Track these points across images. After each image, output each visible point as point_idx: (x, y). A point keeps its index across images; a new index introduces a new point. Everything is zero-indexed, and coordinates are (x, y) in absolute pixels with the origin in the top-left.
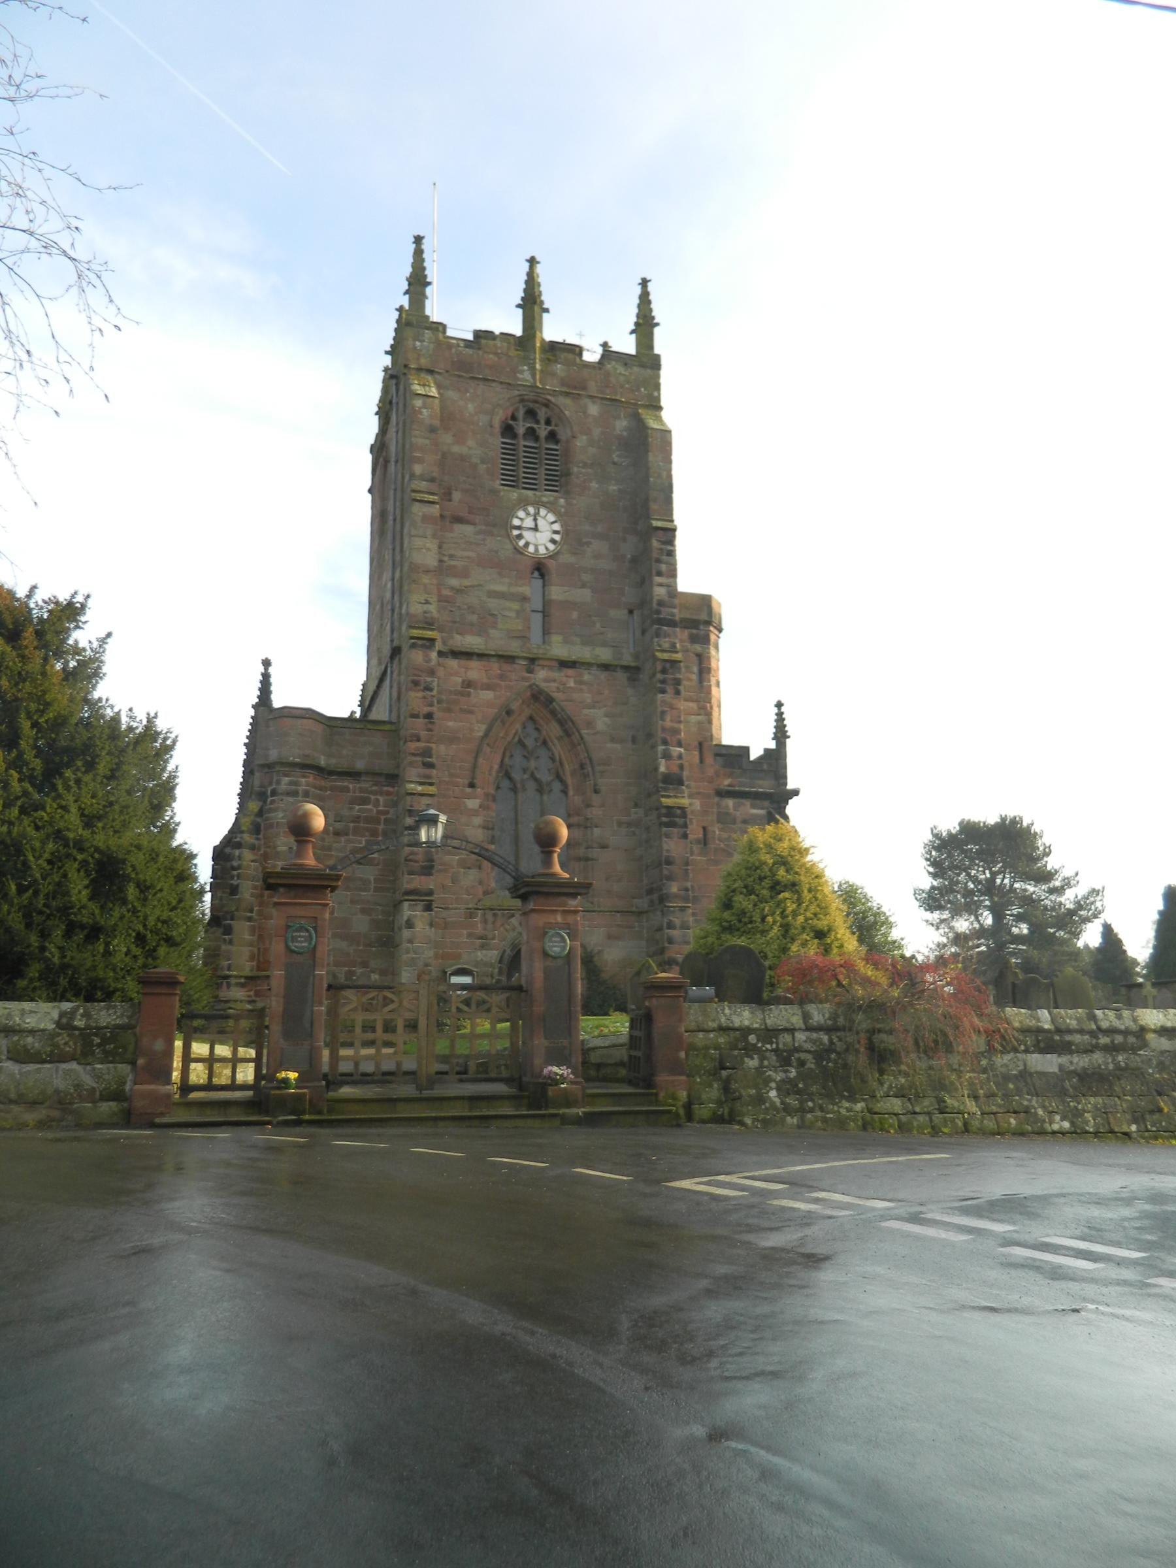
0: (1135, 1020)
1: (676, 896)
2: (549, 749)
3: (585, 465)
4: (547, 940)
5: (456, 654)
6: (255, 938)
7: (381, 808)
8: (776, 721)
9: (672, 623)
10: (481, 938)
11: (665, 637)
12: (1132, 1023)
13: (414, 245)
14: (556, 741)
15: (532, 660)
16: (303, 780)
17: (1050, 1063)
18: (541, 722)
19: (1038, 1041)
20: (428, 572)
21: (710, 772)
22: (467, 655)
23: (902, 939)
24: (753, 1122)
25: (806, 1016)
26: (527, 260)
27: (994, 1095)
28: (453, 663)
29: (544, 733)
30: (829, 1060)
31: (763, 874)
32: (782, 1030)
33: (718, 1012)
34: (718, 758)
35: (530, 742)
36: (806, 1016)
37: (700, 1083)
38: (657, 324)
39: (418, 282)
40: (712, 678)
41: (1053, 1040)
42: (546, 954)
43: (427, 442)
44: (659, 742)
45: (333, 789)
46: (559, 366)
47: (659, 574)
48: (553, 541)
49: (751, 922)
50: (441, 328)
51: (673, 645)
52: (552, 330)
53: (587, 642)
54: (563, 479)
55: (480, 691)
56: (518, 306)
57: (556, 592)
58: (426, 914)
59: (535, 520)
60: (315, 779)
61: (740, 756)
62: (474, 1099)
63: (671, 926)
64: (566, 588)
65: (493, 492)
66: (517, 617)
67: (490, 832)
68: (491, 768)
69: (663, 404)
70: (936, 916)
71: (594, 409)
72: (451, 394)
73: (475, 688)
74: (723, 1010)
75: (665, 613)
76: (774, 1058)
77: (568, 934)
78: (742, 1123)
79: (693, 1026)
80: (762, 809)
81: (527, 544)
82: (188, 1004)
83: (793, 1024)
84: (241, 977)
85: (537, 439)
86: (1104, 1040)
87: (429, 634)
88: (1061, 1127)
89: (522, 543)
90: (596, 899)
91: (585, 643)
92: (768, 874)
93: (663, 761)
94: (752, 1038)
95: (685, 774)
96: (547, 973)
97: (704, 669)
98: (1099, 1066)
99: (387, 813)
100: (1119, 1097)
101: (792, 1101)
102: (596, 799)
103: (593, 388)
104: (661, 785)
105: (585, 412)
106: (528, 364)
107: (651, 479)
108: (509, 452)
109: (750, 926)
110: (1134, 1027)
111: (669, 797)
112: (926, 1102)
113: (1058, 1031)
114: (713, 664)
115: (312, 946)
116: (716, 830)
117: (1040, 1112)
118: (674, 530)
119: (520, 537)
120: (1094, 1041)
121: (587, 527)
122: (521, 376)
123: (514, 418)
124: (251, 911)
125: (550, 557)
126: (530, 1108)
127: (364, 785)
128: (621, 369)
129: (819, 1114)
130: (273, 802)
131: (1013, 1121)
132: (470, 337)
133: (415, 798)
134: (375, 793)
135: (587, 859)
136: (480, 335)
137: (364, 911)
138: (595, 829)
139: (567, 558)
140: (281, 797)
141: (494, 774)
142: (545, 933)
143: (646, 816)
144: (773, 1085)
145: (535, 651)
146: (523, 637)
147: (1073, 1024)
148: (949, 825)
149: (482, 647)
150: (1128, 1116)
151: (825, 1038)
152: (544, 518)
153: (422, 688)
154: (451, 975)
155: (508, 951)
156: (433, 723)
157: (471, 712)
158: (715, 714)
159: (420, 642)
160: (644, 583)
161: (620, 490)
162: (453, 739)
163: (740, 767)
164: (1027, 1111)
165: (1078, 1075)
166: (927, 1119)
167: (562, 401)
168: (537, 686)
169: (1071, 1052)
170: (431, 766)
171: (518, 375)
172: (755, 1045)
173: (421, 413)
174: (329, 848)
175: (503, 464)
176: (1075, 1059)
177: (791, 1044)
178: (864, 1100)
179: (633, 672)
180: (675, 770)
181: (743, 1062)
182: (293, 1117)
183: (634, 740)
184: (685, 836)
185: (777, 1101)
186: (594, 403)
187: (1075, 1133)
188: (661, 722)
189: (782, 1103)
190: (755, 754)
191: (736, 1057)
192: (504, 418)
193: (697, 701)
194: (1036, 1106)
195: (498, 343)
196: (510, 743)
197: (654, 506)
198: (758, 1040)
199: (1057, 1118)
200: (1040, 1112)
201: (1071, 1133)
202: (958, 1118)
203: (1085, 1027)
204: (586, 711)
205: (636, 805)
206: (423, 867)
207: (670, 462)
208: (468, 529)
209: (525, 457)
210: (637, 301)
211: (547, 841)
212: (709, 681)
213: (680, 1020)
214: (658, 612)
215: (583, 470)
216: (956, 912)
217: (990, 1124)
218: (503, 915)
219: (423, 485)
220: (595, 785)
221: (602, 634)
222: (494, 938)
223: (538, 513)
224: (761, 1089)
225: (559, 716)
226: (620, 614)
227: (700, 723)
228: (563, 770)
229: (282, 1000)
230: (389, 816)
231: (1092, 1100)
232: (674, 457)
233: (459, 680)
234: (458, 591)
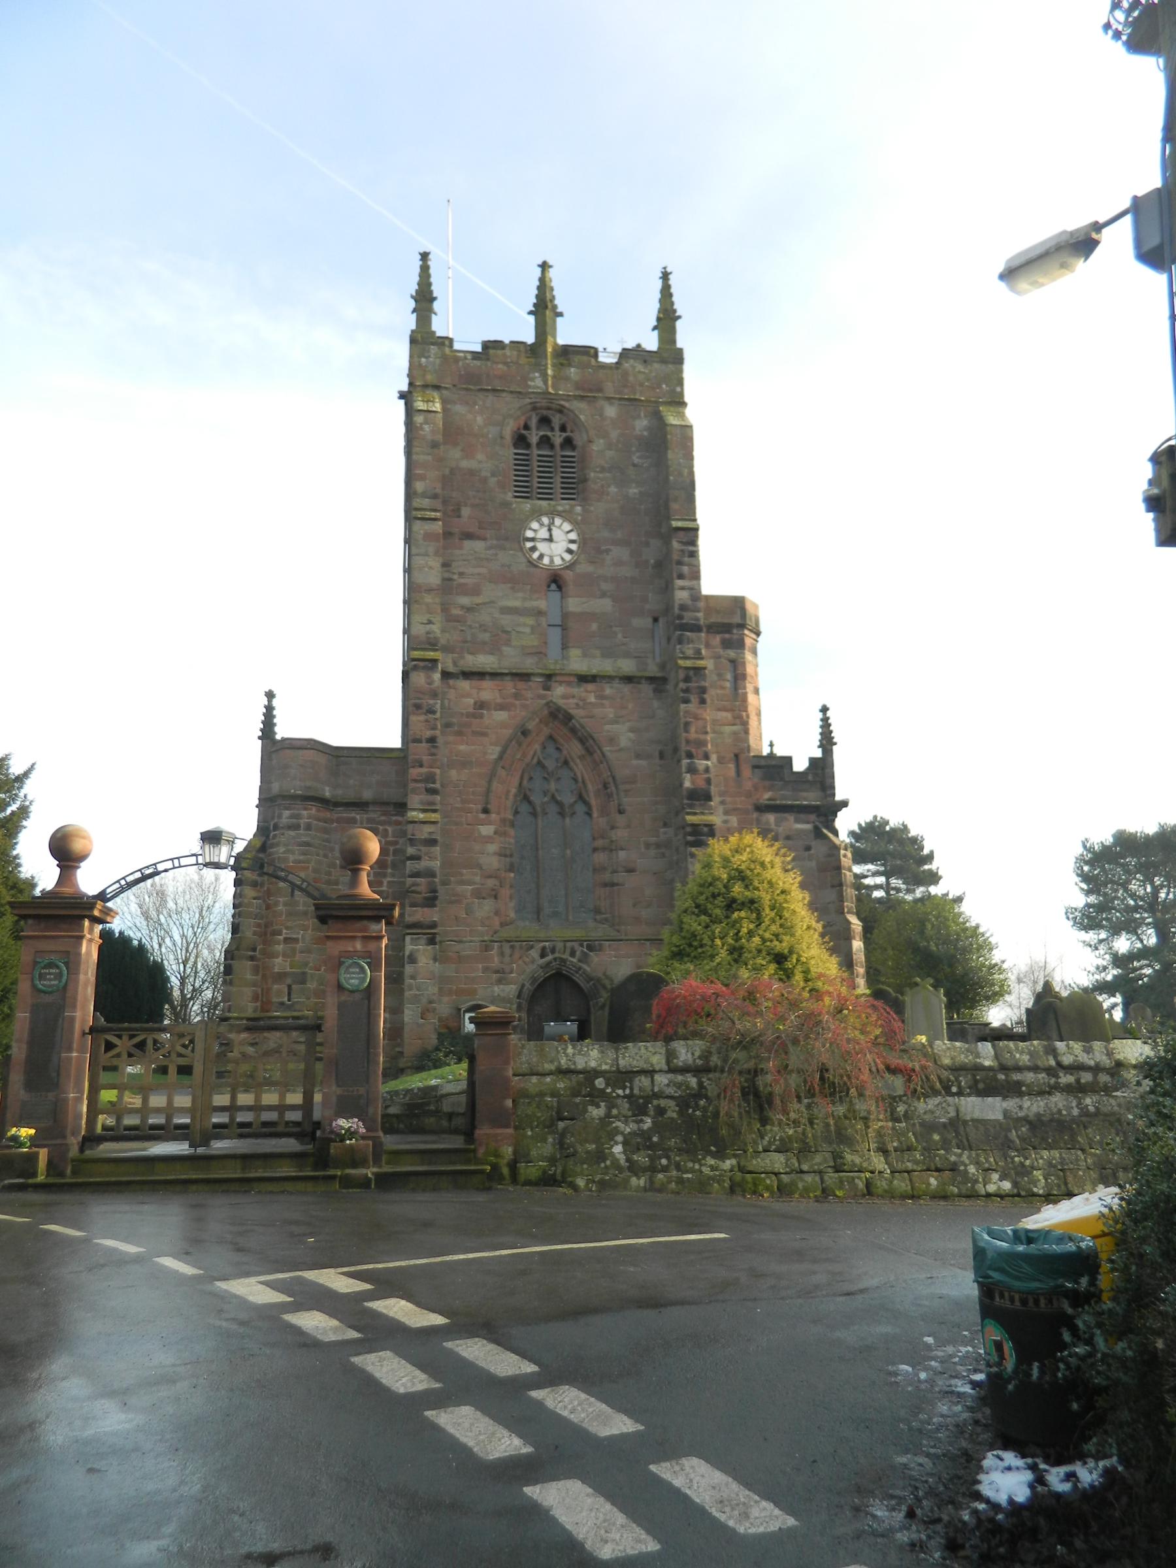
0: (1109, 1054)
2: (571, 769)
3: (603, 470)
4: (342, 970)
5: (467, 675)
6: (259, 977)
7: (390, 839)
8: (821, 727)
9: (696, 628)
10: (497, 972)
11: (688, 643)
12: (1104, 1057)
13: (421, 263)
14: (578, 761)
15: (549, 677)
16: (305, 813)
17: (992, 1109)
18: (561, 740)
19: (976, 1082)
20: (429, 590)
21: (748, 785)
22: (480, 675)
23: (1003, 962)
24: (587, 1184)
25: (670, 1055)
26: (539, 266)
27: (910, 1149)
28: (465, 685)
29: (565, 752)
30: (697, 1107)
31: (716, 891)
32: (637, 1072)
33: (558, 1052)
34: (756, 770)
35: (550, 764)
36: (670, 1055)
37: (532, 1137)
38: (679, 317)
39: (424, 299)
40: (748, 685)
41: (996, 1080)
42: (340, 987)
43: (430, 458)
44: (683, 754)
45: (338, 821)
46: (572, 370)
47: (681, 576)
48: (569, 551)
49: (702, 946)
50: (447, 342)
51: (698, 652)
52: (566, 334)
53: (608, 653)
54: (581, 486)
55: (493, 712)
56: (530, 313)
57: (574, 604)
58: (429, 947)
59: (550, 530)
60: (318, 811)
61: (781, 767)
62: (247, 1159)
64: (584, 600)
65: (506, 504)
66: (532, 633)
67: (508, 859)
68: (508, 792)
69: (686, 399)
70: (1091, 936)
71: (611, 411)
72: (459, 408)
73: (489, 709)
74: (565, 1049)
75: (688, 617)
76: (627, 1106)
77: (369, 964)
78: (575, 1188)
79: (524, 1068)
80: (808, 823)
81: (541, 556)
82: (795, 1041)
83: (652, 1065)
84: (242, 1019)
85: (552, 447)
86: (1066, 1079)
87: (431, 655)
88: (999, 1188)
89: (536, 555)
90: (623, 927)
91: (604, 656)
92: (723, 890)
93: (688, 775)
94: (600, 1083)
95: (713, 790)
96: (341, 1006)
97: (739, 676)
98: (1060, 1111)
99: (396, 843)
100: (1083, 1150)
101: (641, 1158)
102: (621, 820)
103: (609, 389)
104: (686, 801)
105: (601, 415)
106: (540, 371)
107: (671, 478)
108: (522, 463)
109: (700, 950)
110: (1106, 1062)
111: (695, 814)
112: (818, 1158)
113: (1004, 1068)
114: (749, 669)
115: (62, 984)
117: (972, 1169)
118: (696, 530)
119: (534, 549)
120: (1053, 1081)
121: (606, 534)
122: (532, 384)
123: (526, 427)
124: (254, 950)
125: (567, 568)
126: (315, 1169)
127: (372, 815)
128: (640, 367)
129: (674, 1173)
130: (275, 836)
131: (933, 1181)
132: (478, 348)
133: (416, 825)
135: (613, 885)
136: (487, 345)
139: (584, 568)
140: (282, 831)
141: (511, 797)
142: (341, 964)
144: (620, 1138)
145: (552, 667)
146: (540, 654)
147: (1025, 1059)
148: (1103, 836)
149: (495, 666)
150: (1094, 1175)
151: (693, 1081)
152: (559, 527)
153: (424, 711)
154: (465, 1012)
155: (527, 985)
156: (436, 747)
157: (484, 734)
158: (753, 722)
159: (422, 664)
160: (667, 589)
161: (640, 492)
162: (464, 764)
163: (782, 779)
164: (953, 1168)
165: (1030, 1123)
166: (817, 1178)
167: (576, 406)
168: (554, 703)
169: (1021, 1094)
171: (529, 383)
172: (603, 1091)
173: (422, 429)
175: (516, 475)
176: (1026, 1102)
177: (649, 1089)
178: (735, 1156)
179: (658, 683)
180: (701, 784)
181: (586, 1111)
182: (21, 1181)
183: (662, 755)
185: (622, 1158)
186: (611, 404)
187: (1019, 1195)
188: (684, 735)
189: (628, 1160)
191: (577, 1105)
192: (515, 429)
193: (732, 710)
194: (967, 1162)
195: (508, 352)
196: (528, 765)
197: (674, 506)
198: (607, 1085)
199: (995, 1176)
200: (972, 1169)
201: (1013, 1196)
202: (859, 1178)
203: (1039, 1063)
204: (607, 727)
205: (665, 825)
206: (426, 899)
207: (691, 458)
208: (478, 545)
209: (539, 466)
210: (659, 296)
211: (353, 859)
212: (745, 688)
213: (507, 1062)
214: (680, 617)
215: (601, 475)
216: (1116, 930)
217: (901, 1184)
218: (521, 947)
219: (426, 503)
221: (624, 644)
222: (511, 972)
223: (553, 523)
224: (603, 1144)
225: (579, 734)
226: (641, 622)
227: (735, 733)
228: (587, 791)
229: (24, 1046)
230: (398, 847)
231: (1045, 1154)
232: (696, 453)
233: (472, 701)
234: (469, 609)
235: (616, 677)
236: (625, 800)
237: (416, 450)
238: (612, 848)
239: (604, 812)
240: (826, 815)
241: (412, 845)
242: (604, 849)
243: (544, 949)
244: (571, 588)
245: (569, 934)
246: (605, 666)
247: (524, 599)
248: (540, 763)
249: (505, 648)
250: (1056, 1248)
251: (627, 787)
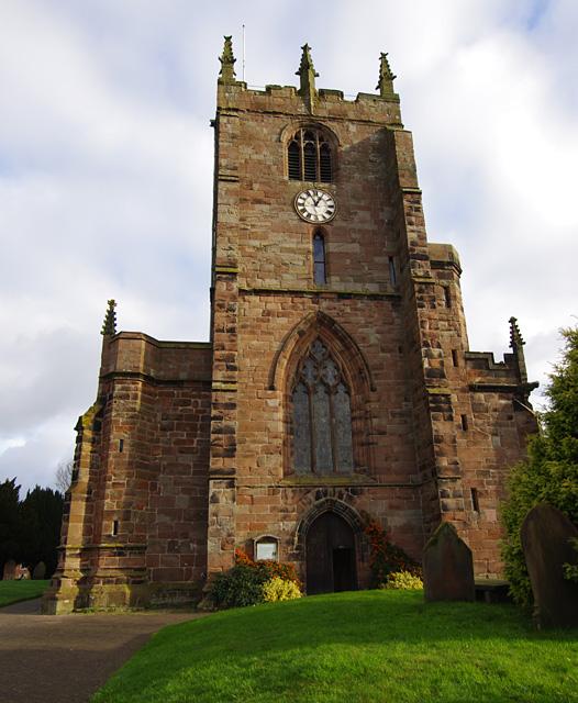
1: (446, 469)
5: (257, 292)
7: (199, 408)
15: (317, 294)
22: (268, 292)
28: (255, 299)
35: (318, 356)
39: (228, 60)
47: (411, 224)
48: (329, 213)
52: (319, 84)
63: (444, 495)
73: (273, 316)
81: (309, 215)
99: (205, 411)
102: (373, 396)
116: (471, 417)
121: (353, 202)
127: (186, 391)
132: (264, 90)
134: (194, 397)
136: (269, 89)
137: (185, 491)
139: (337, 224)
143: (415, 406)
157: (270, 333)
159: (224, 276)
170: (234, 369)
174: (158, 441)
179: (395, 300)
183: (400, 350)
184: (451, 418)
190: (499, 358)
204: (360, 330)
205: (406, 400)
208: (265, 207)
214: (413, 250)
237: (220, 139)
238: (367, 416)
239: (359, 390)
241: (215, 408)
242: (360, 418)
243: (318, 492)
244: (331, 237)
245: (337, 481)
246: (358, 288)
247: (298, 243)
248: (311, 357)
249: (284, 275)
251: (377, 372)
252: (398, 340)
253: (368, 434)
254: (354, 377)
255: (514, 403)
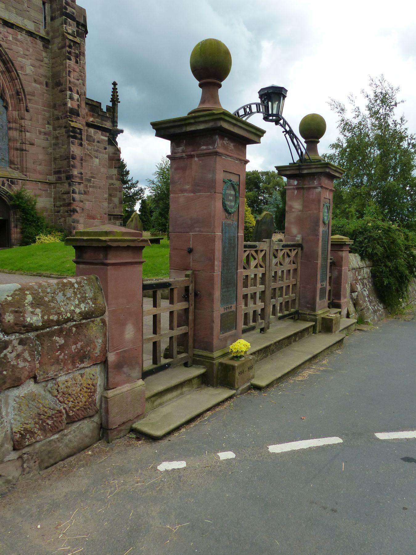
1: (76, 177)
34: (87, 106)
63: (74, 192)
80: (106, 137)
104: (68, 114)
135: (22, 150)
138: (27, 133)
163: (98, 113)
180: (76, 107)
204: (20, 59)
205: (48, 123)
220: (27, 107)
235: (24, 29)
236: (29, 105)
240: (113, 135)
242: (16, 129)
250: (321, 328)
252: (45, 76)
253: (22, 143)
254: (11, 97)
255: (109, 139)
